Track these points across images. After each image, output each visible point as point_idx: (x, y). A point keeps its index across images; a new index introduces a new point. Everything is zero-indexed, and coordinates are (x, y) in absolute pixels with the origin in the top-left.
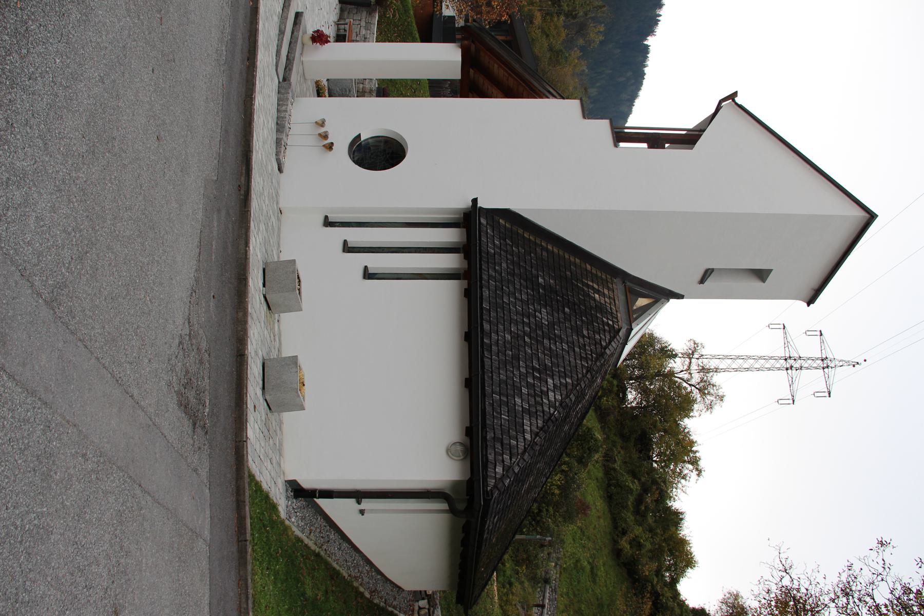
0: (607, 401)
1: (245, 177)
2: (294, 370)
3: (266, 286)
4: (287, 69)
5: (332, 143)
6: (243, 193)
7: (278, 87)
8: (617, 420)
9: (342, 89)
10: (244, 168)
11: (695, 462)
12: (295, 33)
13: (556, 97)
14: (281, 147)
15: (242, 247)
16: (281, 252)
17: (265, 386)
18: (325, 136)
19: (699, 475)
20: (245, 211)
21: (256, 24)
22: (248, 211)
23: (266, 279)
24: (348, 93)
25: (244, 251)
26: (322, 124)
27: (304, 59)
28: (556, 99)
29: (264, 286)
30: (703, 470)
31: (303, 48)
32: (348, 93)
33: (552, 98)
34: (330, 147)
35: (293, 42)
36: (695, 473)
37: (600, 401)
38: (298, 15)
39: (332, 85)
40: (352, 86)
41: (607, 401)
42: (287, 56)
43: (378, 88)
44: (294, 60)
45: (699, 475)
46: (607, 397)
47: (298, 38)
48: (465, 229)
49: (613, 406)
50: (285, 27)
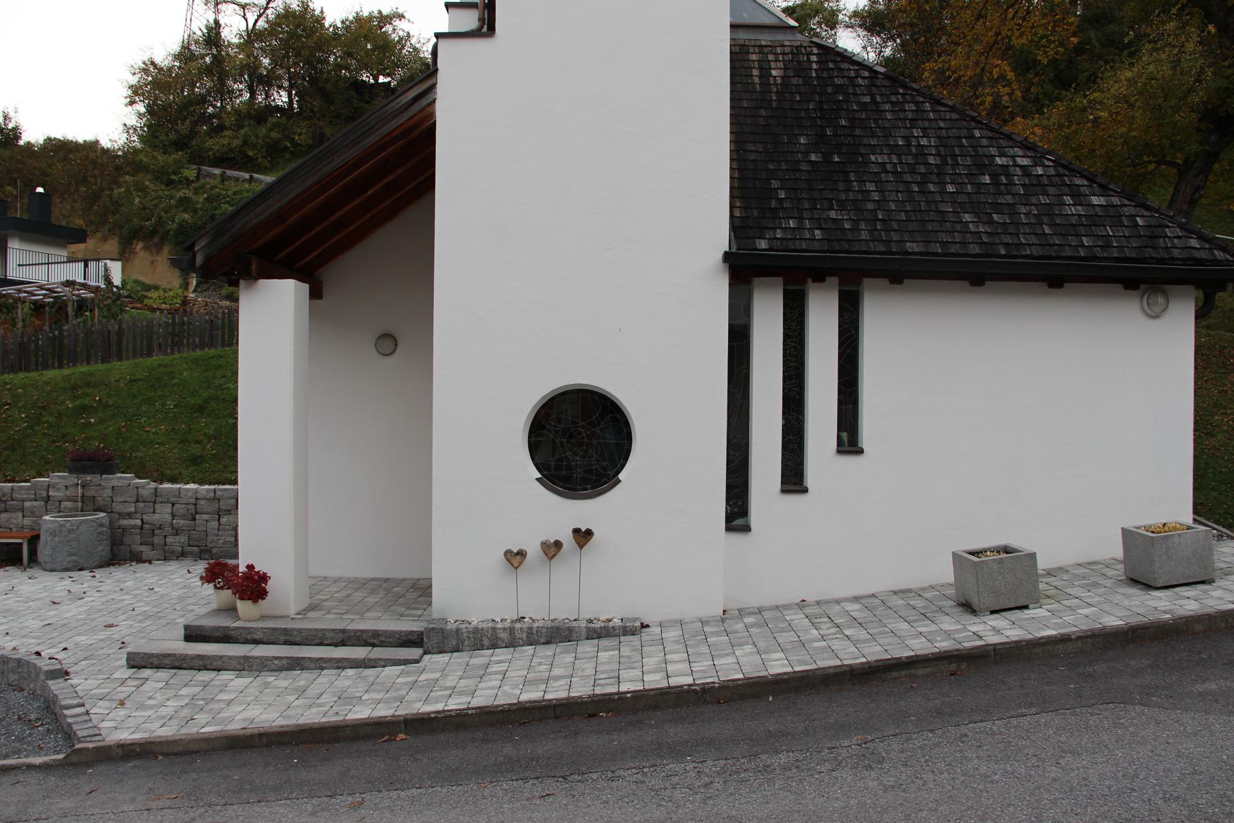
0: (300, 134)
1: (916, 668)
2: (1176, 540)
3: (1025, 604)
4: (375, 641)
5: (576, 531)
6: (954, 665)
7: (440, 653)
8: (331, 123)
9: (99, 541)
10: (895, 674)
11: (385, 19)
12: (255, 636)
13: (434, 86)
14: (613, 627)
15: (1070, 646)
16: (803, 601)
17: (1199, 580)
18: (552, 549)
19: (401, 17)
20: (995, 654)
21: (467, 714)
22: (994, 649)
23: (1012, 606)
24: (105, 529)
25: (1080, 642)
26: (515, 558)
27: (292, 611)
28: (438, 86)
29: (1026, 607)
30: (395, 10)
31: (283, 617)
32: (105, 529)
33: (436, 93)
34: (583, 536)
35: (286, 637)
36: (397, 23)
37: (300, 145)
38: (193, 635)
39: (92, 561)
40: (93, 521)
41: (300, 134)
42: (336, 645)
43: (71, 472)
44: (344, 631)
45: (401, 17)
46: (294, 133)
47: (274, 629)
48: (756, 280)
49: (310, 127)
50: (276, 658)
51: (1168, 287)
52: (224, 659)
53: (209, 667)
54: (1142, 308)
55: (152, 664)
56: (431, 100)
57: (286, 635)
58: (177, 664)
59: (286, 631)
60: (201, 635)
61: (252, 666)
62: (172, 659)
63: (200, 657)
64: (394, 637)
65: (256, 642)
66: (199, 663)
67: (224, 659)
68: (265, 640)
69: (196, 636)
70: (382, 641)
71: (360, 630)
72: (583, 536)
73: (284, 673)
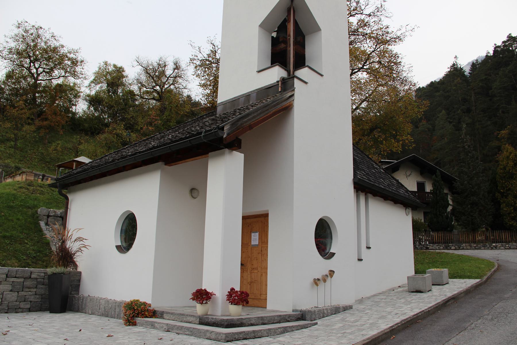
12: (252, 322)
13: (293, 95)
26: (316, 282)
28: (295, 94)
51: (370, 195)
52: (262, 331)
53: (256, 337)
54: (406, 213)
55: (235, 338)
56: (293, 99)
57: (262, 320)
58: (245, 337)
59: (262, 318)
60: (232, 324)
61: (271, 333)
62: (243, 334)
63: (254, 332)
64: (294, 317)
65: (252, 325)
66: (253, 335)
67: (262, 331)
68: (255, 324)
69: (231, 324)
70: (291, 319)
71: (285, 315)
72: (332, 272)
73: (282, 335)
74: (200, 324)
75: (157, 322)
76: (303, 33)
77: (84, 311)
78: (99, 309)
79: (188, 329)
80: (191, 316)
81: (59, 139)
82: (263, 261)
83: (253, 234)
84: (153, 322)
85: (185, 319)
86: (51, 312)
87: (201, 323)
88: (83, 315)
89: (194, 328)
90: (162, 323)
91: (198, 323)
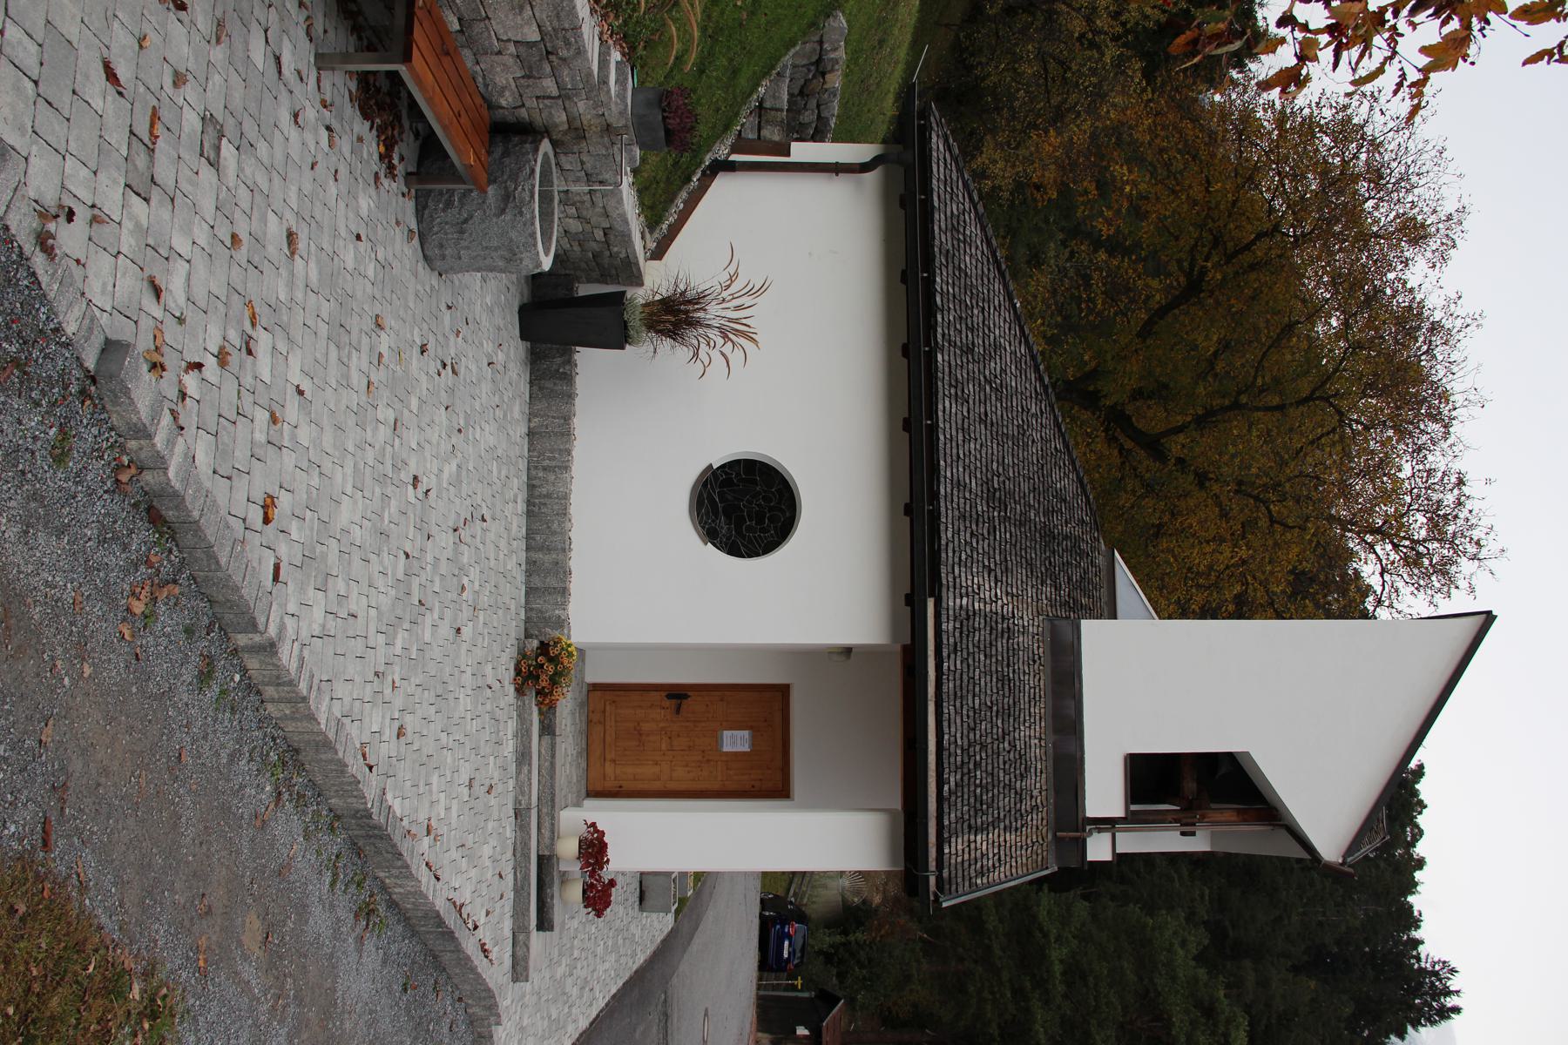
74: (538, 856)
75: (530, 772)
76: (1253, 783)
77: (538, 406)
78: (545, 469)
79: (526, 877)
80: (553, 832)
81: (1035, 127)
82: (687, 766)
83: (746, 734)
84: (531, 757)
85: (545, 810)
86: (524, 311)
87: (540, 858)
88: (524, 388)
89: (529, 894)
90: (530, 792)
91: (541, 853)
